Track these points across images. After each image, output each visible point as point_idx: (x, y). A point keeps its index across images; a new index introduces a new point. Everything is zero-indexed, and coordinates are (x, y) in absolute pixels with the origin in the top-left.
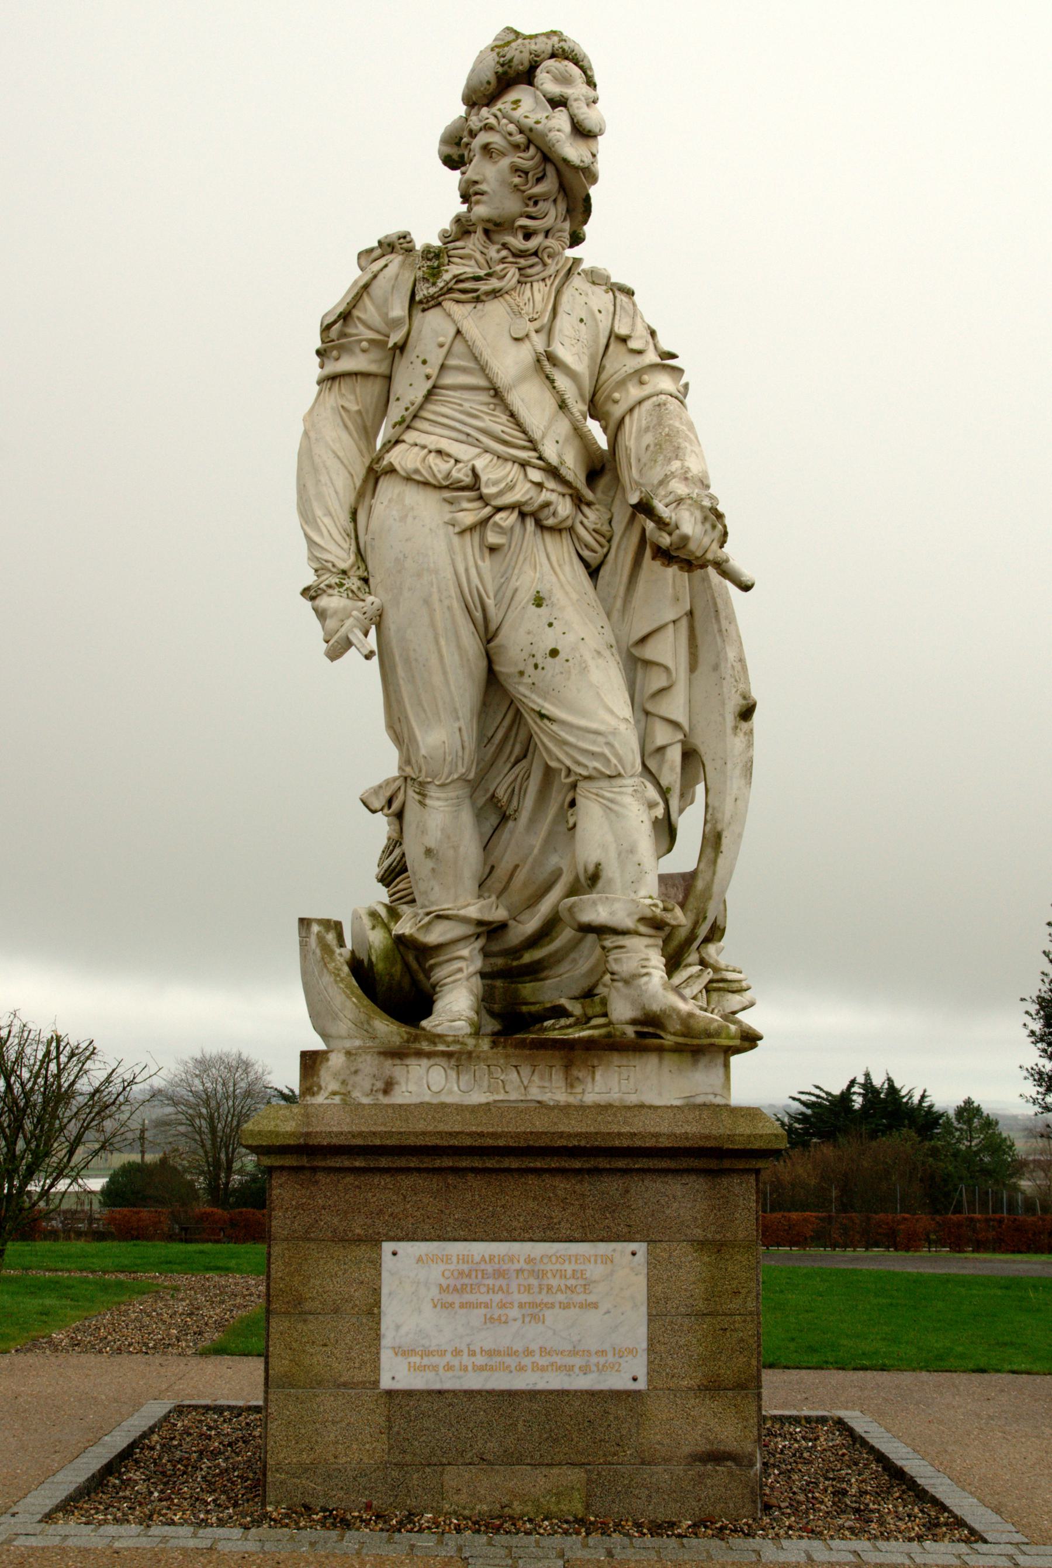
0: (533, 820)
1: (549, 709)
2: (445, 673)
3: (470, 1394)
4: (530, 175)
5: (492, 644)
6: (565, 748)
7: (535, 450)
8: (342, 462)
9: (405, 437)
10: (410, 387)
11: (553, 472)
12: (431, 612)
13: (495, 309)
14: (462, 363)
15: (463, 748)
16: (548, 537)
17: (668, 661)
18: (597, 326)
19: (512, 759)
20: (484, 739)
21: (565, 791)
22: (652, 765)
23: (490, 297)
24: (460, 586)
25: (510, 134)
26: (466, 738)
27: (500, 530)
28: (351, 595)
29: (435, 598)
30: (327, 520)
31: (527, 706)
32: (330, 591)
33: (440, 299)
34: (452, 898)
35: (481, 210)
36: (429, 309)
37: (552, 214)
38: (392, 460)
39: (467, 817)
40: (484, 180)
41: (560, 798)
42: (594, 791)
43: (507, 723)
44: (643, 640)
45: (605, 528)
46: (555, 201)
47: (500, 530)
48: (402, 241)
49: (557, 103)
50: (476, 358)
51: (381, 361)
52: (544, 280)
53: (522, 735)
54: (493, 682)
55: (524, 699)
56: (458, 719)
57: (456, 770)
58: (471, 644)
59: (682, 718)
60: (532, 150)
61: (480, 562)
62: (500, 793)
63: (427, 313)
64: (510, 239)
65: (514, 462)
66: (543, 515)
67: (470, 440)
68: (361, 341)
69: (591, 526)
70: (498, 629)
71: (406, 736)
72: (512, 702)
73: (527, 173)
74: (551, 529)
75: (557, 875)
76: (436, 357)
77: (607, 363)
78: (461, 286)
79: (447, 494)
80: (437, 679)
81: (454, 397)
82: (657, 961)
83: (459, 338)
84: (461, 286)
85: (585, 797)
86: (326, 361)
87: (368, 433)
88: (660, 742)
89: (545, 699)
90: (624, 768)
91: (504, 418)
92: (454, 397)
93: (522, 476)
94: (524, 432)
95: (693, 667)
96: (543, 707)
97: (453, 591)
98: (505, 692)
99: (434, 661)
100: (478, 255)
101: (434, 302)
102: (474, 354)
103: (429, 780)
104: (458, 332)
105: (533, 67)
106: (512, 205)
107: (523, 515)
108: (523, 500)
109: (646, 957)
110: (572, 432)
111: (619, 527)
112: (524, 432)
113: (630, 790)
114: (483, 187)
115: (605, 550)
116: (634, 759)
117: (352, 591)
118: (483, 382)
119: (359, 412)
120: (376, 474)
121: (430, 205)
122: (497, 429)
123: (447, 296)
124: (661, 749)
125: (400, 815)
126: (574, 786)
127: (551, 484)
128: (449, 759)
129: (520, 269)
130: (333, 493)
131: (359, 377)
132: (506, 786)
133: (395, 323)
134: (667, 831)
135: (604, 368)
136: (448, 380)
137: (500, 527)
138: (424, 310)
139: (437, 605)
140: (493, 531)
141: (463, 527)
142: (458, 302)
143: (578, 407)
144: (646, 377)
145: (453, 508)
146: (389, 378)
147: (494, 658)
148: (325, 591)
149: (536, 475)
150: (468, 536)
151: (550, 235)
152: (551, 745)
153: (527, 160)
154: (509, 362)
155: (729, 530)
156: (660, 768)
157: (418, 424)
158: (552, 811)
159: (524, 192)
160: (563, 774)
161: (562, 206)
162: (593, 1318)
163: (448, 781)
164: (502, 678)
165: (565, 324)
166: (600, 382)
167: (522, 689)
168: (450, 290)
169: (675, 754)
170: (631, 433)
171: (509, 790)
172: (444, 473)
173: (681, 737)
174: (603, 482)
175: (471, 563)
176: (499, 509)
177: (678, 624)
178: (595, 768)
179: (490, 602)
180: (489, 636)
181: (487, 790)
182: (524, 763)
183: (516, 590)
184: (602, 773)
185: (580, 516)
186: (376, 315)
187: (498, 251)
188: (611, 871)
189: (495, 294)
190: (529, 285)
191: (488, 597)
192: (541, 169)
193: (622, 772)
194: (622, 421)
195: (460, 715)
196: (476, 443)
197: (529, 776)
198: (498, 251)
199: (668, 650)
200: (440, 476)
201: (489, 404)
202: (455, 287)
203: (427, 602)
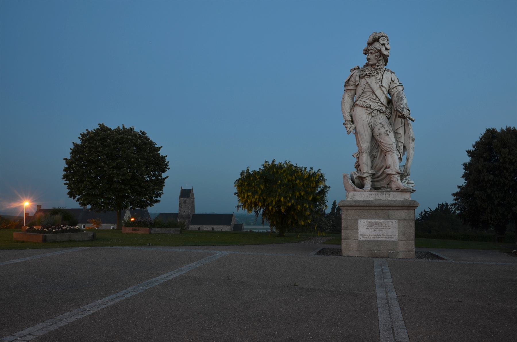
0: (379, 158)
1: (382, 141)
3: (371, 241)
10: (359, 91)
11: (382, 103)
13: (373, 78)
20: (371, 146)
21: (384, 153)
34: (367, 170)
35: (371, 63)
37: (382, 62)
39: (369, 157)
47: (374, 113)
49: (383, 45)
54: (373, 137)
58: (370, 131)
75: (383, 166)
76: (364, 86)
80: (365, 137)
82: (399, 178)
87: (353, 98)
95: (405, 133)
101: (363, 77)
105: (379, 38)
106: (375, 61)
109: (397, 178)
111: (393, 112)
120: (354, 105)
121: (362, 61)
125: (358, 158)
133: (357, 81)
134: (400, 159)
136: (366, 90)
143: (386, 93)
146: (356, 90)
149: (380, 104)
153: (378, 54)
154: (376, 87)
158: (382, 156)
162: (389, 230)
165: (384, 80)
169: (402, 147)
174: (390, 104)
180: (372, 130)
188: (392, 166)
189: (373, 76)
196: (370, 100)
199: (401, 131)
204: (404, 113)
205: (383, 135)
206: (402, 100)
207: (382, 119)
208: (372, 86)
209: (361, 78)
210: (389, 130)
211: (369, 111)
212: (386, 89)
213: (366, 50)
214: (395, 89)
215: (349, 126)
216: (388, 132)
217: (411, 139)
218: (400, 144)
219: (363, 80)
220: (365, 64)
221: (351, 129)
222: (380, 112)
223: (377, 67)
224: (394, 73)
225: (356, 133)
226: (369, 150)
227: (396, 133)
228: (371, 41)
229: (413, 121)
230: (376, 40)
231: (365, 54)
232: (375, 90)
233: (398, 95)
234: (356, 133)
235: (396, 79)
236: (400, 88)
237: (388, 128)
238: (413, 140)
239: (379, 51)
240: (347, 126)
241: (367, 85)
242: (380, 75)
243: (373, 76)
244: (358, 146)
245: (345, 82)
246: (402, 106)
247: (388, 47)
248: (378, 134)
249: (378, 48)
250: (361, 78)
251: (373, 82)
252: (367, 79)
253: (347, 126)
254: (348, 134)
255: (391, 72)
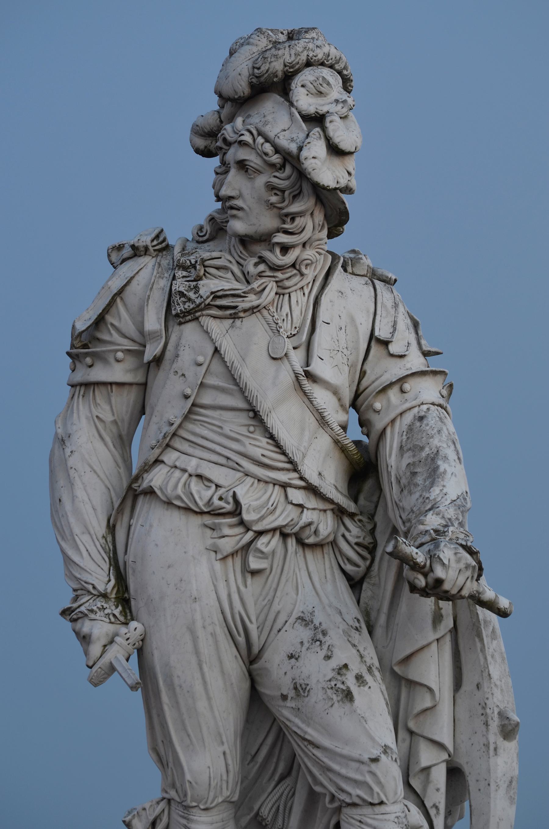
1: (312, 734)
2: (209, 699)
4: (287, 193)
5: (255, 666)
6: (331, 775)
7: (295, 470)
8: (99, 476)
9: (165, 458)
10: (168, 405)
11: (312, 490)
12: (195, 639)
13: (253, 325)
14: (221, 384)
15: (227, 772)
16: (309, 554)
17: (432, 681)
18: (357, 331)
19: (276, 778)
20: (248, 756)
22: (415, 783)
23: (247, 314)
24: (223, 613)
25: (266, 154)
26: (230, 762)
27: (262, 555)
28: (113, 619)
29: (199, 624)
30: (86, 538)
31: (291, 729)
32: (92, 616)
33: (198, 314)
35: (238, 226)
36: (185, 323)
37: (311, 224)
38: (152, 484)
40: (240, 196)
41: (325, 820)
42: (358, 818)
43: (270, 740)
44: (408, 659)
45: (369, 540)
46: (312, 214)
47: (262, 555)
48: (155, 243)
49: (317, 120)
50: (235, 380)
51: (136, 370)
52: (302, 288)
53: (286, 754)
54: (255, 701)
55: (288, 723)
56: (223, 743)
57: (221, 792)
58: (234, 666)
59: (447, 740)
60: (288, 170)
61: (242, 588)
62: (265, 812)
63: (183, 326)
64: (267, 254)
65: (274, 484)
66: (304, 535)
67: (231, 464)
68: (117, 351)
69: (353, 540)
70: (261, 651)
71: (171, 760)
72: (275, 719)
73: (283, 191)
74: (313, 546)
76: (195, 375)
77: (367, 367)
78: (219, 302)
79: (208, 520)
80: (202, 705)
81: (213, 418)
83: (217, 355)
84: (219, 302)
85: (348, 823)
86: (78, 365)
87: (124, 441)
88: (424, 763)
89: (308, 725)
90: (386, 796)
91: (264, 441)
92: (213, 418)
93: (282, 499)
94: (284, 453)
95: (458, 684)
96: (306, 733)
97: (217, 617)
98: (267, 711)
99: (198, 688)
100: (236, 269)
101: (191, 315)
102: (232, 376)
103: (194, 804)
104: (216, 351)
106: (267, 222)
107: (284, 536)
108: (284, 524)
110: (332, 445)
112: (284, 453)
113: (392, 817)
114: (239, 203)
115: (368, 563)
116: (396, 786)
117: (114, 615)
118: (242, 405)
119: (115, 422)
120: (133, 494)
122: (257, 453)
123: (204, 312)
124: (427, 769)
126: (339, 810)
127: (312, 502)
128: (213, 784)
129: (277, 282)
130: (91, 510)
131: (114, 387)
132: (270, 805)
133: (154, 336)
135: (365, 373)
137: (262, 552)
138: (180, 324)
139: (201, 633)
140: (255, 557)
141: (225, 554)
142: (215, 317)
144: (407, 386)
145: (215, 534)
146: (144, 386)
147: (258, 679)
148: (86, 615)
149: (297, 496)
150: (230, 561)
151: (307, 247)
152: (316, 771)
154: (271, 386)
155: (483, 566)
156: (425, 789)
157: (177, 443)
159: (281, 209)
160: (327, 799)
161: (319, 217)
163: (213, 805)
164: (265, 699)
166: (362, 388)
167: (286, 713)
168: (209, 306)
169: (439, 776)
170: (391, 447)
171: (274, 809)
172: (206, 499)
173: (445, 756)
174: (368, 485)
175: (234, 589)
176: (260, 533)
177: (441, 642)
178: (358, 796)
179: (253, 628)
181: (251, 809)
182: (288, 781)
183: (279, 612)
184: (364, 800)
185: (342, 529)
186: (130, 323)
187: (256, 265)
189: (253, 310)
190: (287, 296)
191: (251, 622)
192: (298, 184)
193: (384, 799)
194: (383, 432)
195: (224, 739)
196: (236, 467)
197: (294, 794)
198: (256, 265)
199: (434, 670)
200: (201, 503)
201: (249, 425)
202: (211, 303)
203: (192, 631)
204: (439, 572)
205: (316, 697)
206: (434, 474)
207: (312, 587)
208: (247, 375)
209: (181, 312)
210: (356, 667)
211: (232, 538)
212: (335, 392)
213: (212, 134)
214: (393, 394)
215: (99, 628)
216: (351, 682)
217: (495, 724)
218: (427, 756)
219: (189, 332)
220: (202, 219)
221: (116, 654)
222: (301, 542)
223: (276, 258)
224: (388, 282)
225: (147, 682)
226: (229, 790)
227: (401, 683)
228: (242, 87)
229: (503, 614)
230: (273, 85)
231: (206, 153)
232: (264, 405)
233: (411, 445)
234: (147, 682)
235: (404, 323)
236: (429, 390)
237: (354, 652)
238: (508, 731)
239: (291, 161)
240: (86, 627)
241: (216, 366)
242: (300, 303)
243: (253, 310)
244: (162, 762)
245: (77, 336)
246: (432, 521)
247: (345, 134)
248: (287, 689)
249: (284, 142)
250: (181, 312)
251: (248, 345)
252: (216, 327)
253: (86, 627)
254: (96, 682)
255: (374, 276)
